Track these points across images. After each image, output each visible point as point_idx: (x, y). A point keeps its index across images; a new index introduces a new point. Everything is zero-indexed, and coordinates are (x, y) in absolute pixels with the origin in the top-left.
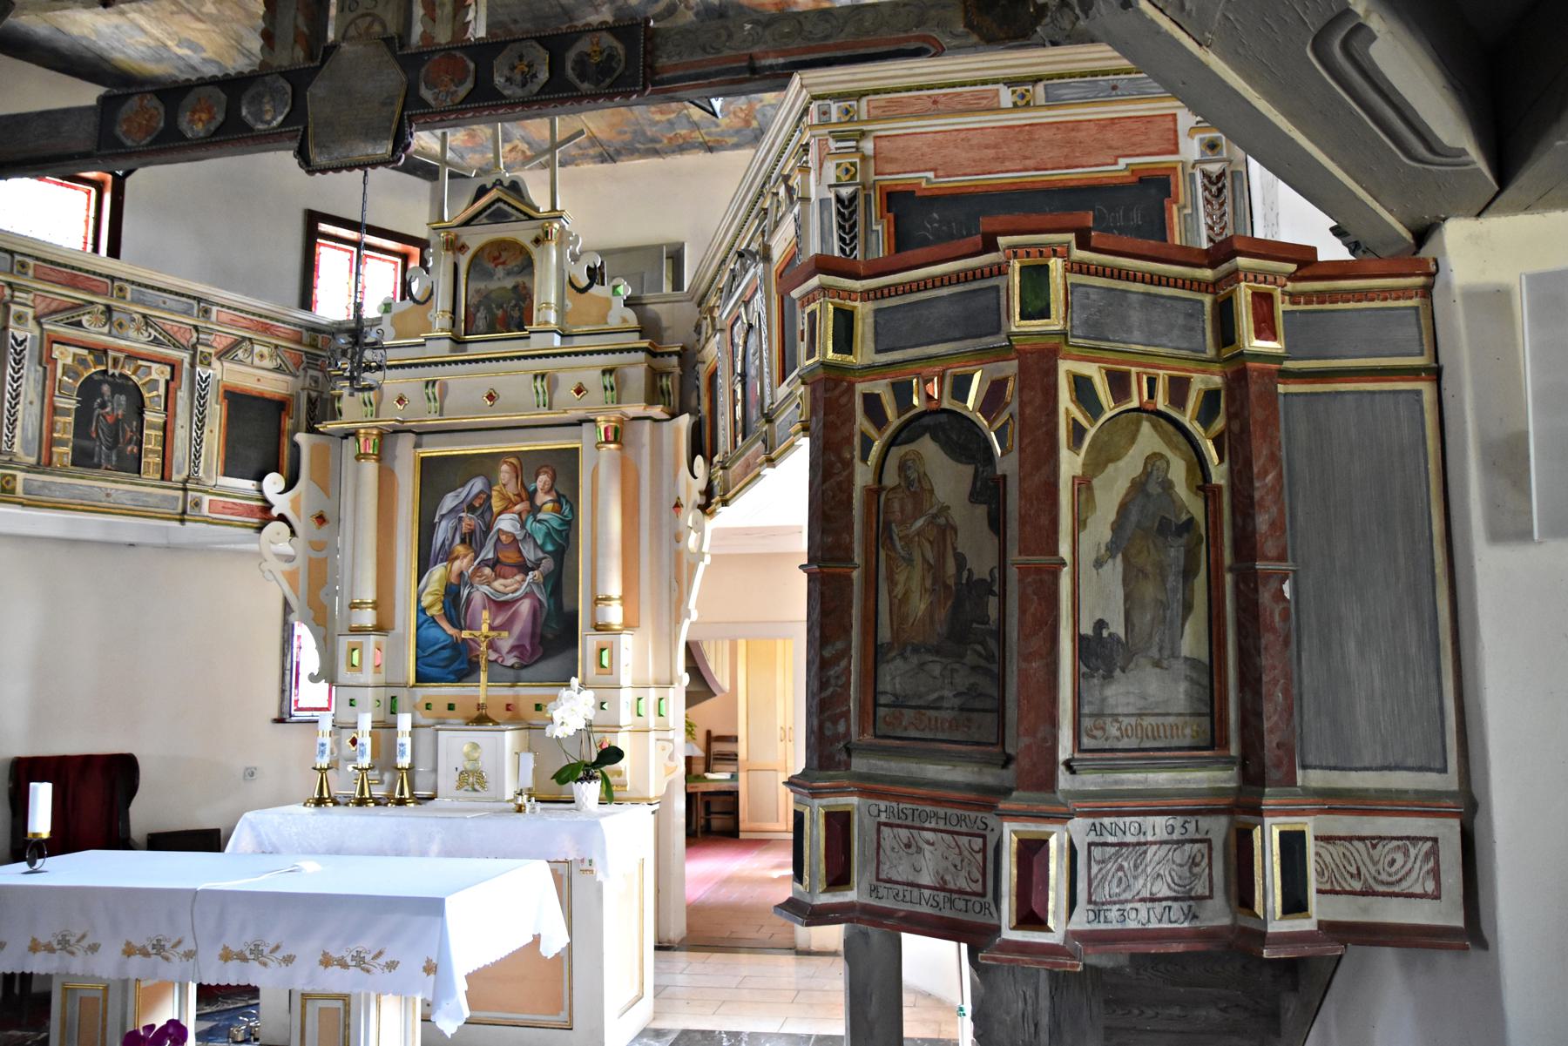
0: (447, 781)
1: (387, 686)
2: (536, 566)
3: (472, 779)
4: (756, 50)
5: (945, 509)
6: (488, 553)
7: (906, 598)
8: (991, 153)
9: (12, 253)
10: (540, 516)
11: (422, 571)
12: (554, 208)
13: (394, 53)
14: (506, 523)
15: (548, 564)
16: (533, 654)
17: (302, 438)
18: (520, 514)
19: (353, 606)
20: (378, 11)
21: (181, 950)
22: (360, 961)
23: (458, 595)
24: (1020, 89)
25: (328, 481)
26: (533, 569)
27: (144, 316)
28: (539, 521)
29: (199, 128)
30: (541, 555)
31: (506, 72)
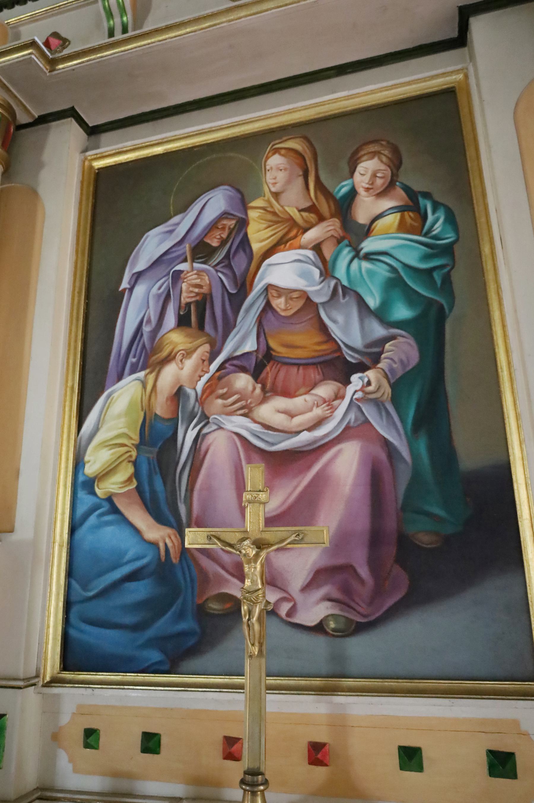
2: (371, 357)
6: (244, 340)
10: (368, 245)
11: (89, 388)
14: (286, 272)
16: (378, 592)
18: (317, 248)
23: (171, 441)
26: (362, 368)
28: (368, 257)
30: (379, 331)
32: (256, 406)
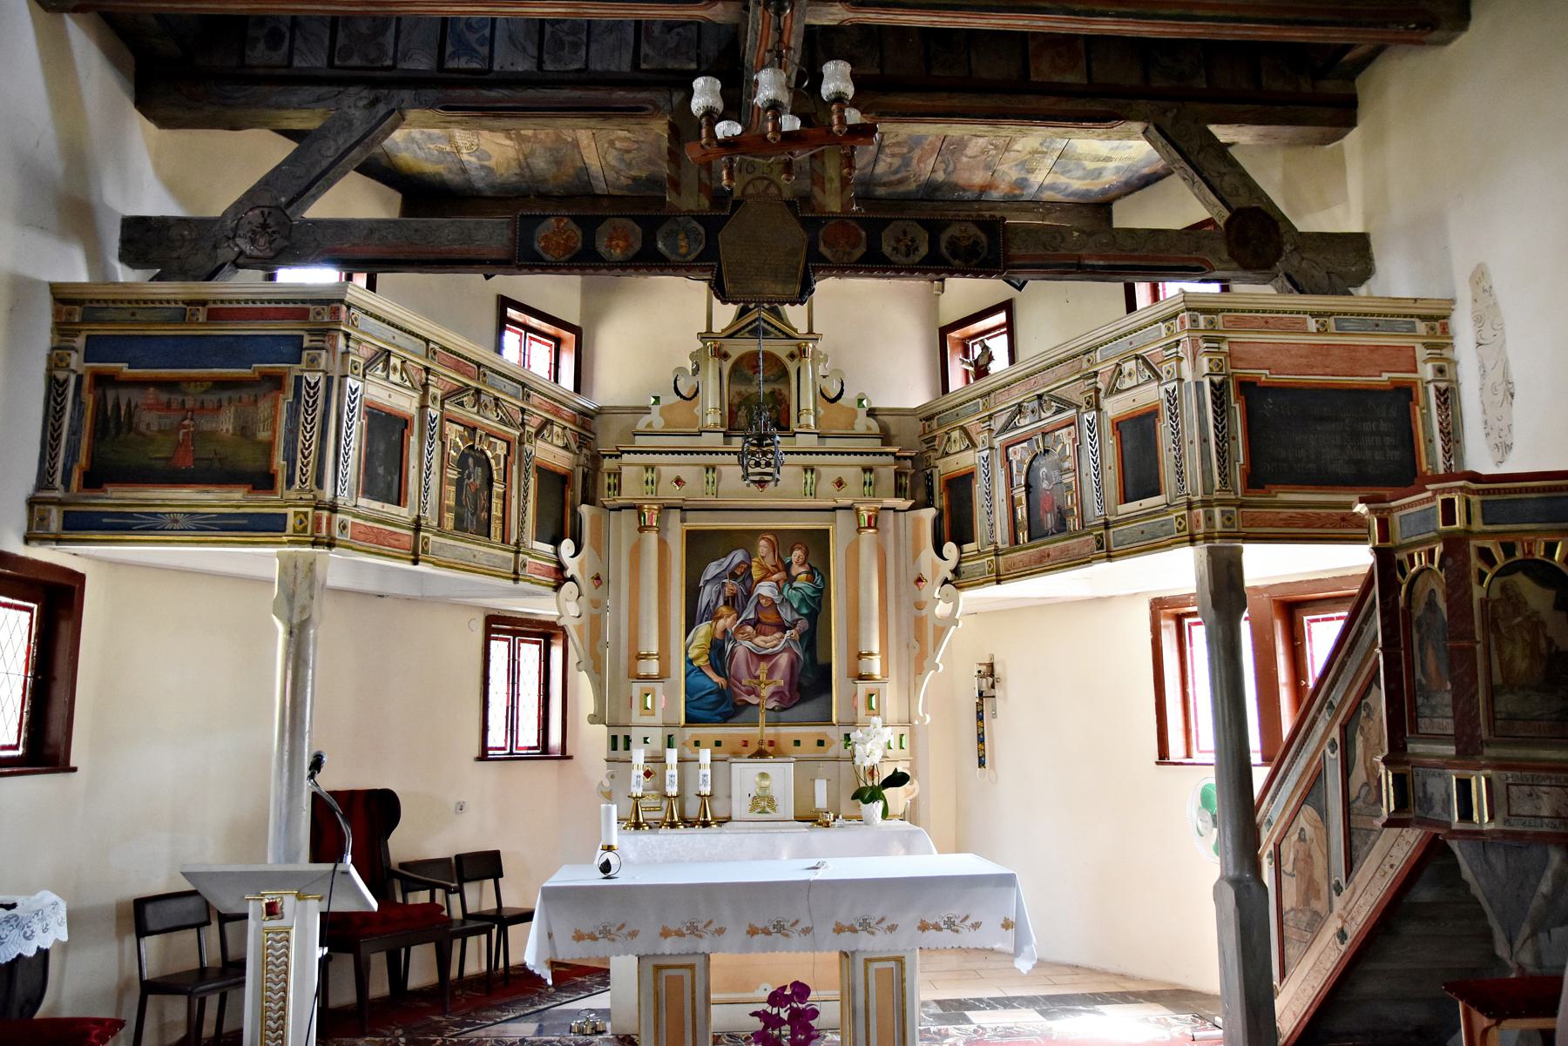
0: (740, 807)
1: (666, 726)
2: (793, 625)
3: (763, 803)
4: (1083, 252)
5: (1536, 613)
7: (1511, 660)
8: (1304, 361)
9: (427, 341)
12: (810, 331)
13: (795, 214)
14: (765, 589)
15: (803, 624)
17: (585, 509)
19: (639, 657)
20: (774, 176)
21: (799, 927)
22: (950, 924)
23: (722, 649)
24: (1321, 320)
25: (600, 547)
27: (497, 399)
29: (617, 253)
31: (893, 243)
32: (290, 203)
